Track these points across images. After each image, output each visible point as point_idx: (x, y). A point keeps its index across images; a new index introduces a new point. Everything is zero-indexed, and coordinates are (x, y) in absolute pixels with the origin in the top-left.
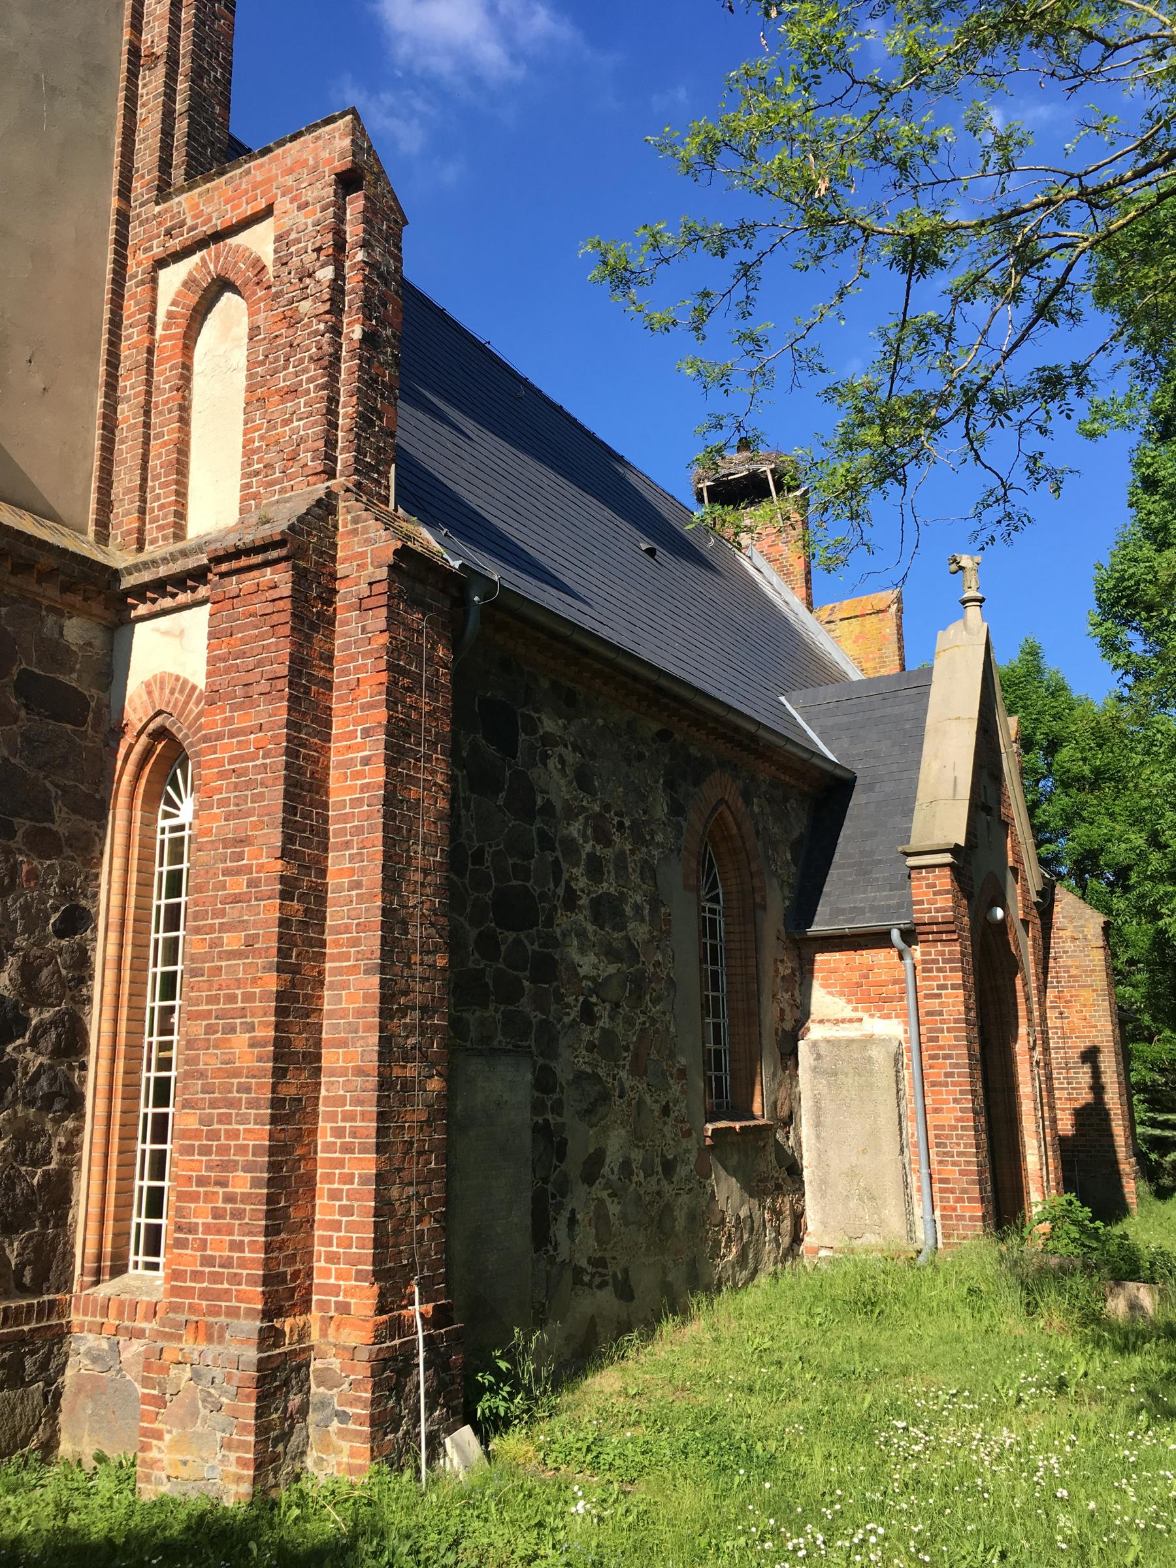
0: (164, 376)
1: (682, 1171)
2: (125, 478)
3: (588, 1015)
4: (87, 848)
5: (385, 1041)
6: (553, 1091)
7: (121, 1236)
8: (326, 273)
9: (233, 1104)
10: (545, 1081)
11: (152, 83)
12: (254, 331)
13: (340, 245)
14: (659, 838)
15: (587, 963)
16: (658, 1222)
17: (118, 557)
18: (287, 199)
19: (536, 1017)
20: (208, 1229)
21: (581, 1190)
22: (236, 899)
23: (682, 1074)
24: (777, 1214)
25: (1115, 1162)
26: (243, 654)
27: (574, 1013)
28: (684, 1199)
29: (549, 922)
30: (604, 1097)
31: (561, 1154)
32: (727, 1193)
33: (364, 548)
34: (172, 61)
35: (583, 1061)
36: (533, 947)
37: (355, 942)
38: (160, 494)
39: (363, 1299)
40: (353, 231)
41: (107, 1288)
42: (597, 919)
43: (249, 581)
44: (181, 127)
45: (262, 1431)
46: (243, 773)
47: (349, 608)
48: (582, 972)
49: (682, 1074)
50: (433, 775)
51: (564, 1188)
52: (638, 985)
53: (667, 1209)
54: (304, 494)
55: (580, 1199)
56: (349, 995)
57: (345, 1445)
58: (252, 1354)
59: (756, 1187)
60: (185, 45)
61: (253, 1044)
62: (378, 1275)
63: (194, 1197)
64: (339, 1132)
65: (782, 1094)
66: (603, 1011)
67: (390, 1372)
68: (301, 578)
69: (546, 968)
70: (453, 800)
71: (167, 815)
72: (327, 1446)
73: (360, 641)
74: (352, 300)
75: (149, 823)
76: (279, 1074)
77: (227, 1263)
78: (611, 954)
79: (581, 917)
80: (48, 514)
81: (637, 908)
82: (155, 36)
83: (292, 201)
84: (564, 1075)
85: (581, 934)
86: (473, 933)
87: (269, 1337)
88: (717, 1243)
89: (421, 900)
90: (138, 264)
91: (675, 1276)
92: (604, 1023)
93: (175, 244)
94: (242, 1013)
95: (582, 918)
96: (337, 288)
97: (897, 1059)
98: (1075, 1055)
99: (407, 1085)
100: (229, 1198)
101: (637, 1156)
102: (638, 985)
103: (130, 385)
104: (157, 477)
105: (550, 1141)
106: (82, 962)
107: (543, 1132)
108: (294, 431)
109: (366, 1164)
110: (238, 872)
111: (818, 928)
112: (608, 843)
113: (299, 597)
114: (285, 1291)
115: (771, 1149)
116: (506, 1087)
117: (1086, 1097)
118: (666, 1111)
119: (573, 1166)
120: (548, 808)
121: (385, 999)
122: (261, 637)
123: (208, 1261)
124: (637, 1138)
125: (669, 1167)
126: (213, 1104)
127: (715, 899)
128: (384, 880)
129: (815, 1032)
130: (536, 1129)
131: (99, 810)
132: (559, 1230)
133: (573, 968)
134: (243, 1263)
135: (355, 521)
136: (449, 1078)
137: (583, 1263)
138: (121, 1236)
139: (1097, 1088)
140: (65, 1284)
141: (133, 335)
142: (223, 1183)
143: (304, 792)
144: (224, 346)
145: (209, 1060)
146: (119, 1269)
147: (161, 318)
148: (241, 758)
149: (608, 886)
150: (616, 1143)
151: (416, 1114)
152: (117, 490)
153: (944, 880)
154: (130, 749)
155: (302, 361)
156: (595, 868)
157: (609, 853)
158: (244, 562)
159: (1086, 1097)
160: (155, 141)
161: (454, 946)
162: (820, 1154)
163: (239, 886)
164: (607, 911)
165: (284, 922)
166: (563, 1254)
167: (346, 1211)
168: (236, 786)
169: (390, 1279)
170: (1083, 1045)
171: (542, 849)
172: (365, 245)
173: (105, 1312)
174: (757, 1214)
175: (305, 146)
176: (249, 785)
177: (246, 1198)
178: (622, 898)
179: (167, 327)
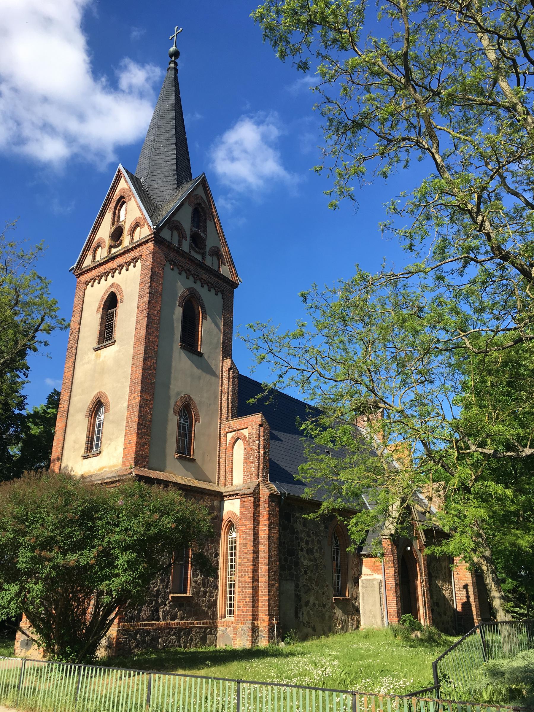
0: (229, 454)
1: (327, 607)
2: (222, 473)
3: (306, 573)
4: (218, 542)
5: (269, 577)
7: (225, 611)
8: (257, 442)
10: (297, 586)
11: (225, 397)
12: (245, 449)
13: (259, 437)
14: (322, 534)
15: (306, 562)
16: (322, 617)
17: (222, 489)
21: (305, 608)
23: (327, 586)
24: (353, 620)
25: (473, 619)
27: (303, 572)
28: (328, 613)
30: (309, 590)
31: (300, 601)
32: (338, 613)
33: (264, 494)
34: (228, 393)
35: (305, 582)
38: (228, 476)
39: (267, 619)
40: (262, 434)
41: (223, 620)
42: (307, 553)
43: (246, 499)
44: (230, 405)
45: (252, 638)
49: (327, 586)
50: (276, 530)
51: (301, 607)
52: (317, 567)
53: (324, 614)
54: (254, 482)
55: (304, 609)
56: (263, 569)
58: (250, 626)
59: (346, 613)
60: (230, 389)
62: (269, 615)
65: (354, 592)
66: (309, 572)
67: (271, 630)
68: (255, 499)
69: (297, 564)
70: (279, 535)
72: (262, 642)
73: (264, 509)
74: (262, 447)
75: (227, 537)
76: (253, 582)
78: (311, 560)
80: (209, 481)
81: (317, 550)
82: (225, 387)
84: (301, 585)
85: (304, 556)
86: (283, 557)
87: (253, 624)
88: (336, 624)
89: (274, 553)
90: (223, 432)
91: (326, 629)
92: (309, 574)
93: (230, 430)
95: (304, 553)
96: (259, 445)
97: (380, 584)
98: (462, 588)
99: (273, 585)
101: (317, 602)
102: (317, 567)
103: (222, 455)
105: (298, 598)
107: (296, 595)
109: (267, 597)
111: (363, 552)
112: (310, 537)
113: (254, 503)
114: (255, 617)
115: (351, 604)
116: (290, 586)
117: (465, 599)
118: (323, 594)
119: (303, 603)
120: (297, 532)
121: (269, 570)
124: (317, 599)
125: (324, 606)
127: (338, 546)
128: (169, 383)
129: (363, 577)
131: (219, 535)
133: (302, 563)
136: (279, 584)
138: (225, 611)
139: (468, 597)
140: (217, 619)
141: (223, 446)
143: (256, 535)
144: (239, 449)
145: (242, 580)
146: (225, 617)
149: (310, 546)
150: (312, 600)
151: (274, 590)
153: (389, 542)
154: (224, 523)
156: (307, 543)
157: (310, 539)
159: (465, 599)
160: (226, 409)
161: (280, 560)
162: (364, 606)
163: (246, 551)
164: (310, 551)
166: (301, 620)
169: (271, 616)
170: (464, 584)
172: (264, 436)
174: (347, 619)
178: (313, 548)
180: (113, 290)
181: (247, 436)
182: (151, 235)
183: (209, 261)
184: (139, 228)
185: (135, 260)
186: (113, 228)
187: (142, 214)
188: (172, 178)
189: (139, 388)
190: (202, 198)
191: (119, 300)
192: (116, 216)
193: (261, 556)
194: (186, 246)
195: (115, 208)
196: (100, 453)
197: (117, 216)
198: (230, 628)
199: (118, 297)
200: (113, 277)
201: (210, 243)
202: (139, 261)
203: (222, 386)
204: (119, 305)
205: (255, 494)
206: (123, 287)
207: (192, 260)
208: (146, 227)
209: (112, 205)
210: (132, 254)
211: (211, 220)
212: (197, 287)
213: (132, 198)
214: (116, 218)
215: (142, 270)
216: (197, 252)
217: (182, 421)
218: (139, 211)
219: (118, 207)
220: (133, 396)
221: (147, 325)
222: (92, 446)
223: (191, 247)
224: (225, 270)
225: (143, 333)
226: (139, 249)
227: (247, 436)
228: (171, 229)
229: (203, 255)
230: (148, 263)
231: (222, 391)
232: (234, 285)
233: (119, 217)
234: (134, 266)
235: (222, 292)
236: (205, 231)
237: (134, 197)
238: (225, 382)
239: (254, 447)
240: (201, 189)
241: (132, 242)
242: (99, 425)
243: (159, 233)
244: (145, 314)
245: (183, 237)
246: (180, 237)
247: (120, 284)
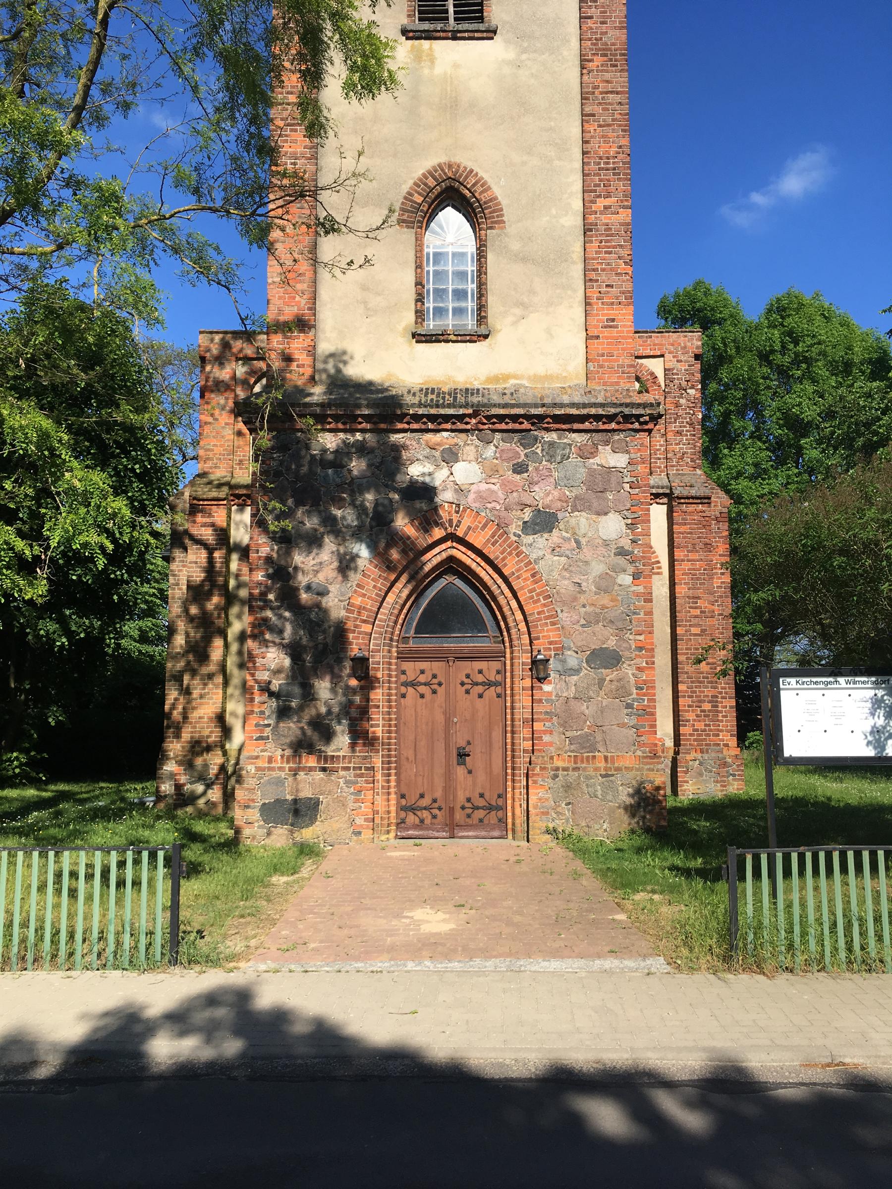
18: (671, 355)
20: (694, 720)
22: (696, 617)
26: (691, 533)
43: (691, 508)
57: (736, 783)
83: (674, 357)
100: (704, 711)
108: (681, 449)
110: (696, 608)
122: (700, 528)
142: (700, 707)
148: (694, 569)
155: (683, 422)
158: (691, 501)
168: (692, 579)
175: (679, 337)
176: (698, 579)
177: (709, 711)
239: (683, 401)
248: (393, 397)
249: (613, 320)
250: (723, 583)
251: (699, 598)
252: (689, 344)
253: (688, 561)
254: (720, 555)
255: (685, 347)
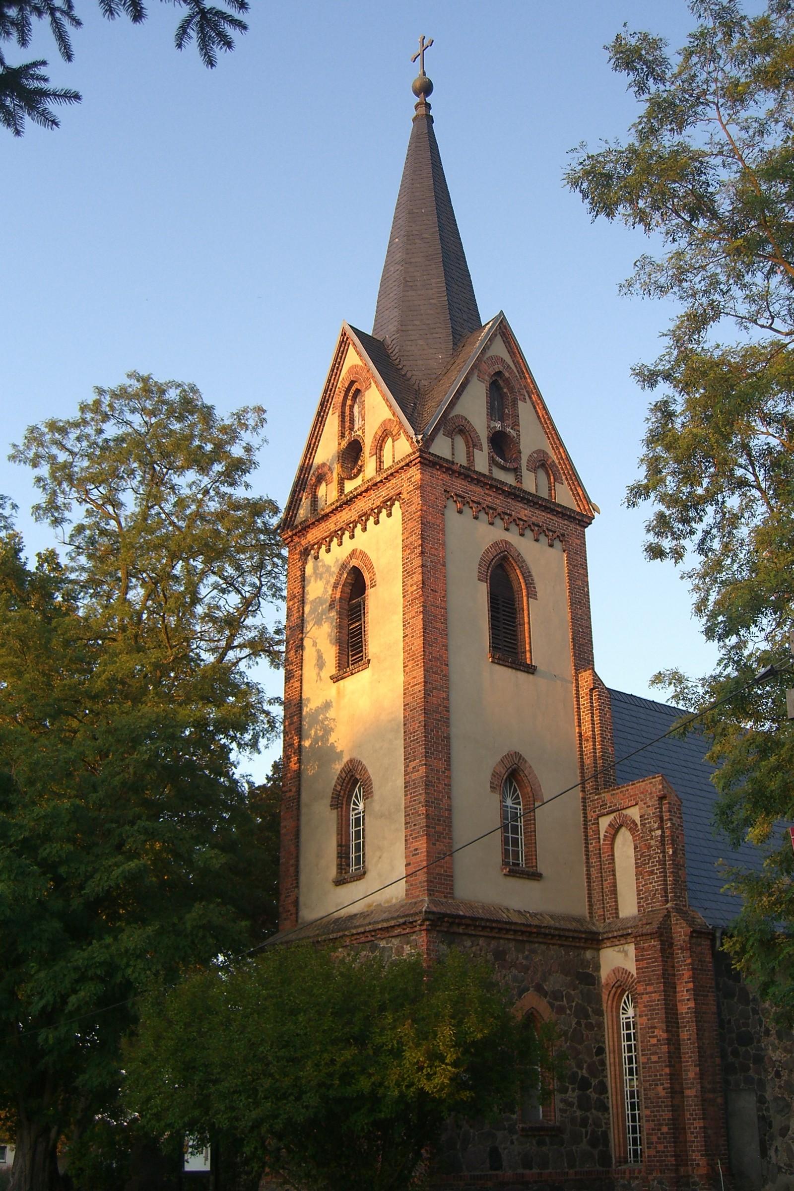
3: (778, 1075)
6: (765, 1103)
8: (659, 832)
9: (660, 1106)
10: (761, 1100)
17: (600, 927)
19: (756, 1077)
20: (657, 1143)
22: (654, 1045)
26: (647, 968)
27: (773, 1074)
29: (759, 1041)
31: (771, 1127)
36: (752, 1052)
37: (691, 1057)
46: (652, 1006)
47: (678, 949)
48: (774, 1059)
61: (664, 1089)
63: (652, 1134)
64: (691, 1115)
68: (662, 943)
69: (759, 1059)
71: (354, 809)
75: (618, 1017)
77: (663, 1152)
79: (772, 1038)
86: (730, 1049)
90: (591, 815)
94: (660, 1080)
95: (773, 1039)
96: (663, 836)
100: (662, 1134)
104: (607, 895)
106: (603, 1063)
108: (654, 886)
110: (653, 1037)
113: (663, 950)
120: (754, 1000)
123: (658, 1152)
126: (654, 1107)
130: (759, 1117)
132: (772, 1153)
133: (770, 1058)
134: (668, 1152)
135: (677, 920)
137: (782, 1165)
145: (651, 1094)
147: (602, 837)
148: (651, 1001)
152: (594, 900)
165: (669, 1052)
166: (774, 1160)
167: (696, 1137)
171: (754, 1014)
173: (625, 1173)
176: (654, 1010)
177: (667, 1133)
179: (604, 840)
180: (354, 562)
181: (639, 823)
182: (414, 453)
183: (530, 483)
184: (390, 441)
185: (388, 504)
186: (344, 443)
187: (394, 414)
188: (443, 333)
189: (421, 750)
190: (503, 361)
191: (368, 582)
192: (346, 422)
193: (685, 1049)
194: (482, 464)
195: (344, 404)
196: (365, 873)
197: (347, 418)
198: (637, 1182)
199: (367, 576)
200: (352, 537)
201: (530, 440)
202: (397, 503)
203: (580, 726)
204: (370, 592)
205: (663, 934)
206: (372, 556)
207: (497, 487)
208: (403, 437)
209: (338, 399)
210: (383, 493)
211: (524, 400)
212: (512, 537)
213: (373, 384)
214: (347, 424)
215: (404, 522)
216: (503, 468)
217: (509, 802)
218: (387, 409)
219: (349, 402)
220: (412, 764)
221: (424, 628)
222: (350, 865)
223: (492, 462)
224: (564, 496)
225: (418, 642)
226: (393, 481)
227: (639, 823)
228: (450, 434)
229: (516, 471)
230: (413, 508)
231: (580, 735)
232: (583, 520)
233: (352, 421)
234: (389, 515)
235: (562, 538)
236: (516, 425)
237: (375, 382)
238: (586, 717)
239: (653, 842)
240: (499, 340)
241: (379, 469)
242: (358, 820)
243: (428, 447)
244: (418, 607)
245: (474, 446)
246: (468, 447)
247: (367, 551)
248: (377, 905)
249: (416, 849)
250: (689, 1008)
251: (655, 1027)
252: (654, 789)
253: (647, 994)
254: (686, 982)
255: (651, 793)
